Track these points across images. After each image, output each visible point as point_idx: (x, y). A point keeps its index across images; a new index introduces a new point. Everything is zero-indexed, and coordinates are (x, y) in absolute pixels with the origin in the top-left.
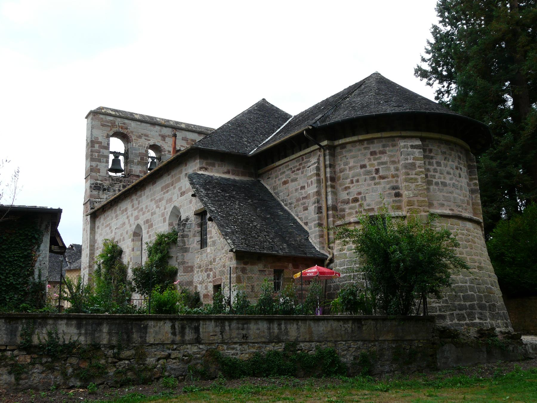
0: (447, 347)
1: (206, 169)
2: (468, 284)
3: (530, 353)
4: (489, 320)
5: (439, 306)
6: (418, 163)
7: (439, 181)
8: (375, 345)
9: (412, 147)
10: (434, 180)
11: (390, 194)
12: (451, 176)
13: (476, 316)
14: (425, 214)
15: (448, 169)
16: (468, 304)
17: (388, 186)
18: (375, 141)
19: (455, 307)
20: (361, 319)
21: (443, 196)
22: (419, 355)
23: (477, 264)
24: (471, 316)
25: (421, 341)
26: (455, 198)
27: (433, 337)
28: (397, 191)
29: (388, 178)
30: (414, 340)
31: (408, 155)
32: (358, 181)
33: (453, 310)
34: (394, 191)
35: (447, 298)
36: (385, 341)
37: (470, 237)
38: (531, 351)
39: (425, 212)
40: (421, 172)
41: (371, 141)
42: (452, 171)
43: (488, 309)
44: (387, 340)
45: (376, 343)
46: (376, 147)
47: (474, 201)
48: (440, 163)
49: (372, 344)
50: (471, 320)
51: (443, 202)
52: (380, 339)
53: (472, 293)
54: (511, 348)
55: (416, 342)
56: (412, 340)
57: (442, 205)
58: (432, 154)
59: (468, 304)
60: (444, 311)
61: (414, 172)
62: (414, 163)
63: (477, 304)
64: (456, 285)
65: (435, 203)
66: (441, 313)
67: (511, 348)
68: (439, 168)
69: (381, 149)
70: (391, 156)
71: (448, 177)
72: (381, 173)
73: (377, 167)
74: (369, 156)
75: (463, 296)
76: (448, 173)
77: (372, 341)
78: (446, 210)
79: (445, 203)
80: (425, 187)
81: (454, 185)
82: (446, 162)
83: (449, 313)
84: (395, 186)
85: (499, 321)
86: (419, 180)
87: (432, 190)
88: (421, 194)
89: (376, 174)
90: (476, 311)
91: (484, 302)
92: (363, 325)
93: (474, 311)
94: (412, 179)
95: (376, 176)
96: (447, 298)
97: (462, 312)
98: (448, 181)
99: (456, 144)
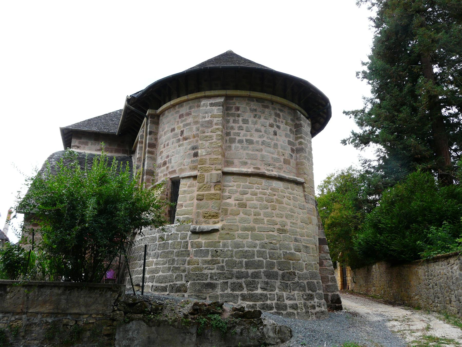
0: (133, 325)
1: (78, 147)
2: (258, 248)
3: (269, 337)
4: (277, 291)
5: (211, 273)
6: (215, 120)
7: (244, 138)
8: (21, 319)
9: (212, 105)
10: (238, 138)
11: (189, 154)
12: (261, 134)
13: (259, 286)
14: (217, 172)
15: (258, 126)
16: (250, 271)
17: (189, 147)
18: (184, 104)
19: (233, 274)
20: (6, 285)
21: (247, 154)
22: (88, 334)
23: (277, 227)
24: (252, 285)
25: (94, 316)
26: (263, 157)
27: (114, 311)
28: (196, 151)
29: (190, 138)
30: (83, 314)
31: (206, 113)
32: (168, 145)
33: (229, 278)
34: (194, 152)
35: (224, 264)
36: (37, 313)
37: (275, 197)
38: (271, 334)
39: (217, 170)
40: (218, 129)
41: (180, 104)
42: (263, 129)
43: (279, 278)
44: (41, 313)
45: (24, 316)
46: (184, 110)
47: (298, 161)
48: (248, 120)
49: (17, 317)
50: (250, 290)
51: (246, 160)
52: (30, 311)
53: (261, 259)
54: (238, 330)
55: (86, 316)
56: (80, 314)
57: (245, 164)
58: (239, 112)
59: (250, 271)
60: (216, 279)
61: (210, 130)
62: (211, 120)
63: (264, 272)
64: (240, 249)
65: (236, 161)
66: (212, 282)
67: (238, 330)
68: (245, 126)
69: (188, 111)
70: (195, 117)
71: (256, 134)
72: (185, 134)
73: (182, 129)
74: (178, 119)
75: (246, 262)
76: (257, 130)
77: (18, 314)
78: (249, 168)
79: (249, 161)
80: (220, 144)
81: (263, 143)
82: (255, 120)
83: (222, 281)
84: (195, 146)
85: (296, 292)
86: (215, 137)
87: (233, 148)
88: (215, 151)
89: (181, 136)
90: (260, 280)
91: (276, 269)
92: (7, 293)
93: (256, 280)
94: (207, 137)
95: (181, 137)
96: (224, 264)
97: (239, 281)
98: (255, 139)
99: (272, 102)
